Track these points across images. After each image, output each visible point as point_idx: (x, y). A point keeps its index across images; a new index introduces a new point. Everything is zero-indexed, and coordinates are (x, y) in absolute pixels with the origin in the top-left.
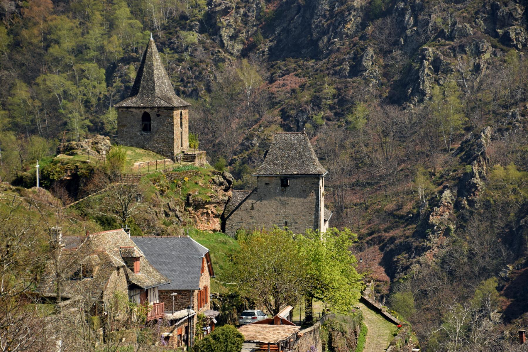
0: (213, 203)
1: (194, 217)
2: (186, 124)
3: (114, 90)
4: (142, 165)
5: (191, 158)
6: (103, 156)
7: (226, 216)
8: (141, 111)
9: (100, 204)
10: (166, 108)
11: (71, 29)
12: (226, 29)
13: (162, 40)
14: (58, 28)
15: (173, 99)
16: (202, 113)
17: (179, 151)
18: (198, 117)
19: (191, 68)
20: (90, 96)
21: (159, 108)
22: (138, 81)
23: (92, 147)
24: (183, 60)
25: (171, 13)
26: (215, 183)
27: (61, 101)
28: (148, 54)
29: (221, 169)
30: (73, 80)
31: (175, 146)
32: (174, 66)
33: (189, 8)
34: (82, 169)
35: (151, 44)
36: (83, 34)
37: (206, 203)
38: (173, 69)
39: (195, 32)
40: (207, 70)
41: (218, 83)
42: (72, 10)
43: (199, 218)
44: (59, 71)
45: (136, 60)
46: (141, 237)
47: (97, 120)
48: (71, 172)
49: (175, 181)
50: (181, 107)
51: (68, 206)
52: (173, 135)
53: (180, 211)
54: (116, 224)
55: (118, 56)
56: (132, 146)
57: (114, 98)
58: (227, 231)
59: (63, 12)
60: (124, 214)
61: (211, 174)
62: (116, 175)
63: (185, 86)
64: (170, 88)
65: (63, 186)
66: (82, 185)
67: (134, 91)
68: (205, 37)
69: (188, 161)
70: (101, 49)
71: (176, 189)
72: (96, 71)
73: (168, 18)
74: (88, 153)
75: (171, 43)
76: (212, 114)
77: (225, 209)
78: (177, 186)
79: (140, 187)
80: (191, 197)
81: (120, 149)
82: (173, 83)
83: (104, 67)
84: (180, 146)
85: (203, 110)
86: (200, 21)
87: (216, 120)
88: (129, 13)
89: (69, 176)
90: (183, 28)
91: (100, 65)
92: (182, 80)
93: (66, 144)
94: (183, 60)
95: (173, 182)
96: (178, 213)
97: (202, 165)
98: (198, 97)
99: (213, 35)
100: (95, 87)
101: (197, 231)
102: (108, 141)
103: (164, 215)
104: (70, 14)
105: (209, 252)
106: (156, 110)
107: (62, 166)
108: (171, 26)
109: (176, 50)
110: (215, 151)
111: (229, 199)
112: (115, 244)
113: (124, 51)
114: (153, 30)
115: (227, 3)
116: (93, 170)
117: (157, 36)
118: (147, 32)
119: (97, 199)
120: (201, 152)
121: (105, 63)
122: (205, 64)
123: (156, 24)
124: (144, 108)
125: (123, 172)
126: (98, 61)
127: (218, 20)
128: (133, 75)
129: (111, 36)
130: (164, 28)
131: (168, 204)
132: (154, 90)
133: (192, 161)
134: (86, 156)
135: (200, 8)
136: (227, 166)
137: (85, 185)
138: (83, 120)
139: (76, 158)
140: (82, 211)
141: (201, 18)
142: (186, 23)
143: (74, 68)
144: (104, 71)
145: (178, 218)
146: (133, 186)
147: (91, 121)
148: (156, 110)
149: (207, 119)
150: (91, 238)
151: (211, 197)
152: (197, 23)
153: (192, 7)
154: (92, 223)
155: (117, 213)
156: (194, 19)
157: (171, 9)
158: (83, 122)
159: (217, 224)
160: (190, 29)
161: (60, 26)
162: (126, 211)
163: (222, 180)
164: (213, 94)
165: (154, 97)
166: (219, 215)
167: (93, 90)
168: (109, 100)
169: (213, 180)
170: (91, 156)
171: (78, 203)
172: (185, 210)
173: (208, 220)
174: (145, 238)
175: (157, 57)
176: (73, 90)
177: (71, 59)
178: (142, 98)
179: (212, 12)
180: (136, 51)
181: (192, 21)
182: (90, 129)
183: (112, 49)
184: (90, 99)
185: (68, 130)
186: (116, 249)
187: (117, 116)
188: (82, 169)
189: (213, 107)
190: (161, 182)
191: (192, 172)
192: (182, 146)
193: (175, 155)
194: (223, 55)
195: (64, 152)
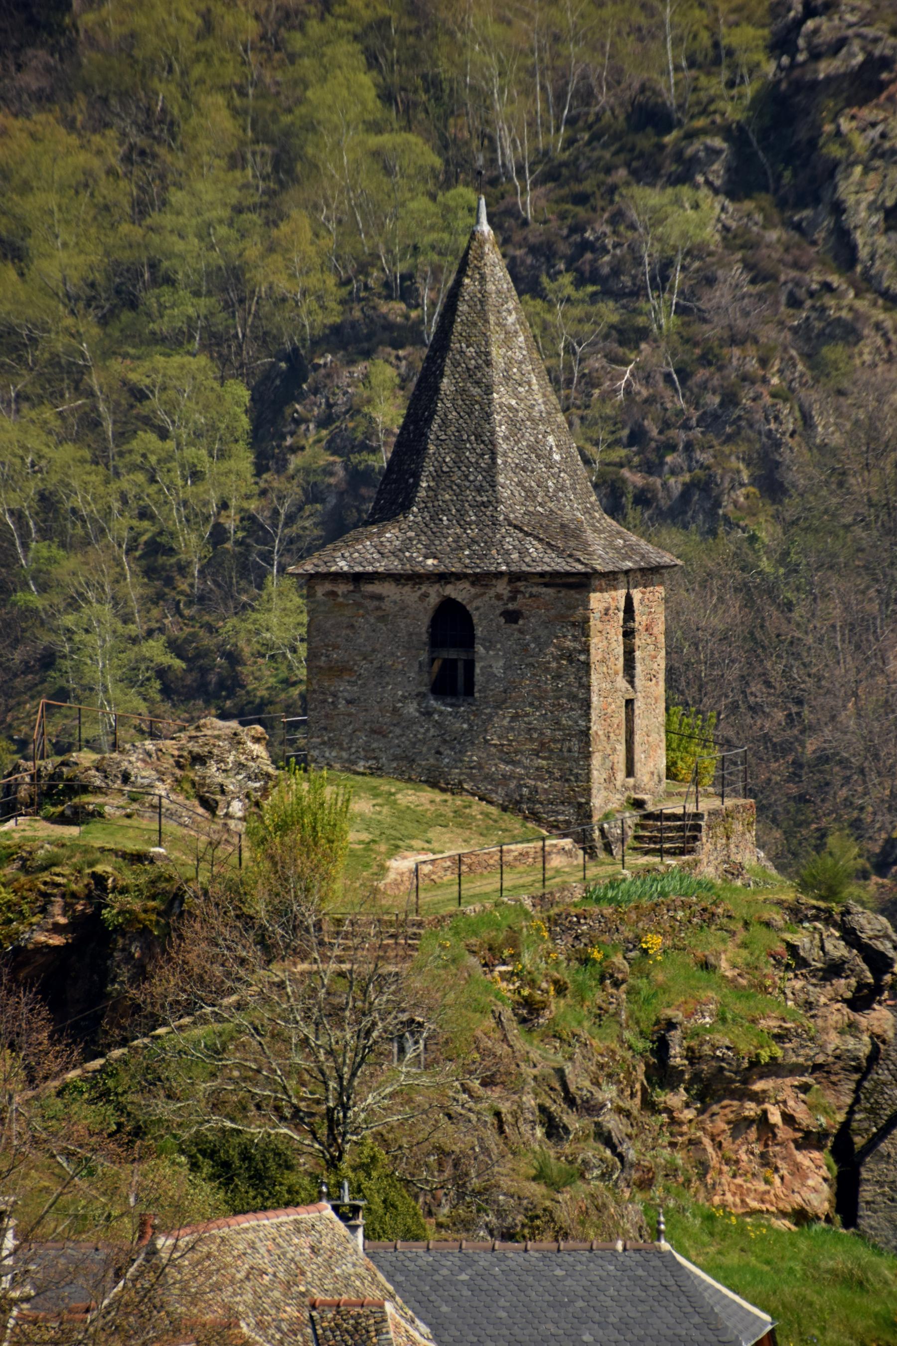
0: (796, 1070)
1: (694, 1143)
2: (652, 661)
3: (295, 491)
4: (426, 869)
5: (676, 835)
6: (232, 824)
7: (859, 1141)
8: (426, 595)
9: (213, 1075)
10: (553, 579)
11: (85, 183)
12: (866, 171)
13: (535, 233)
14: (16, 181)
15: (590, 535)
16: (735, 604)
17: (616, 801)
18: (715, 621)
19: (684, 374)
20: (174, 518)
21: (515, 577)
22: (412, 440)
23: (177, 781)
24: (643, 334)
25: (586, 96)
26: (803, 963)
27: (25, 546)
28: (463, 307)
29: (831, 893)
30: (90, 438)
31: (598, 775)
32: (596, 362)
33: (677, 68)
34: (124, 891)
35: (481, 257)
36: (141, 209)
37: (759, 1068)
38: (590, 381)
39: (704, 191)
40: (765, 381)
41: (823, 447)
42: (87, 88)
43: (720, 1146)
44: (21, 397)
45: (401, 336)
46: (418, 1248)
47: (208, 641)
48: (67, 908)
49: (597, 955)
50: (627, 572)
51: (54, 1084)
52: (587, 716)
53: (620, 1110)
54: (291, 1178)
55: (315, 318)
56: (374, 772)
57: (294, 530)
58: (867, 1219)
59: (44, 99)
60: (332, 1123)
61: (778, 918)
62: (295, 926)
63: (651, 468)
64: (573, 475)
65: (28, 985)
66: (125, 973)
67: (392, 494)
68: (759, 217)
69: (661, 852)
70: (230, 282)
71: (598, 996)
72: (202, 395)
73: (571, 122)
74: (157, 808)
75: (586, 246)
76: (789, 606)
77: (857, 1101)
78: (607, 977)
79: (417, 983)
80: (675, 1036)
81: (316, 790)
82: (591, 450)
83: (243, 372)
84: (621, 775)
85: (743, 588)
86: (736, 135)
87: (810, 640)
88: (370, 95)
89: (57, 929)
90: (647, 171)
91: (224, 361)
92: (637, 437)
93: (49, 765)
94: (643, 334)
95: (585, 961)
96: (612, 1123)
97: (734, 871)
98: (714, 523)
99: (800, 203)
100: (196, 475)
101: (710, 1218)
102: (258, 749)
103: (539, 1132)
104: (80, 110)
105: (772, 1333)
106: (502, 587)
107: (23, 879)
108: (584, 164)
109: (606, 285)
110: (802, 799)
111: (875, 1050)
112: (288, 1285)
113: (344, 291)
114: (490, 182)
115: (876, 40)
116: (178, 897)
117: (512, 212)
118: (463, 193)
119: (205, 1046)
120: (729, 802)
121: (249, 350)
122: (752, 350)
123: (510, 151)
124: (443, 578)
125: (328, 907)
126: (215, 342)
127: (828, 128)
128: (389, 413)
129: (282, 216)
130: (552, 174)
131: (560, 1073)
132: (493, 485)
133: (682, 852)
134: (144, 823)
135: (734, 67)
136: (864, 875)
137: (141, 975)
138: (134, 640)
139: (96, 837)
140: (120, 1109)
141: (739, 116)
142: (661, 147)
143: (94, 380)
144: (245, 395)
145: (613, 1148)
146: (381, 981)
147: (175, 647)
148: (502, 587)
149: (758, 634)
150: (165, 1255)
151: (779, 1038)
152: (717, 142)
153: (692, 64)
154: (170, 1175)
155: (297, 1118)
156: (701, 122)
157: (584, 77)
158: (132, 654)
159: (813, 1182)
160: (684, 178)
161: (26, 171)
162: (346, 1108)
163: (838, 949)
164: (791, 507)
165: (495, 523)
166: (824, 1134)
167: (189, 490)
168: (267, 539)
169: (792, 948)
170: (170, 826)
171: (102, 1070)
172: (649, 1105)
173: (765, 1160)
174: (435, 1252)
175: (511, 319)
176: (86, 488)
177: (75, 333)
178: (432, 529)
179: (798, 86)
180: (406, 290)
181: (690, 136)
182: (171, 689)
183: (283, 285)
184: (172, 535)
185: (63, 694)
186: (291, 1311)
187: (305, 619)
188: (124, 891)
189: (794, 570)
190: (526, 959)
191: (684, 906)
192: (630, 772)
193: (596, 817)
194: (847, 302)
195: (34, 806)
